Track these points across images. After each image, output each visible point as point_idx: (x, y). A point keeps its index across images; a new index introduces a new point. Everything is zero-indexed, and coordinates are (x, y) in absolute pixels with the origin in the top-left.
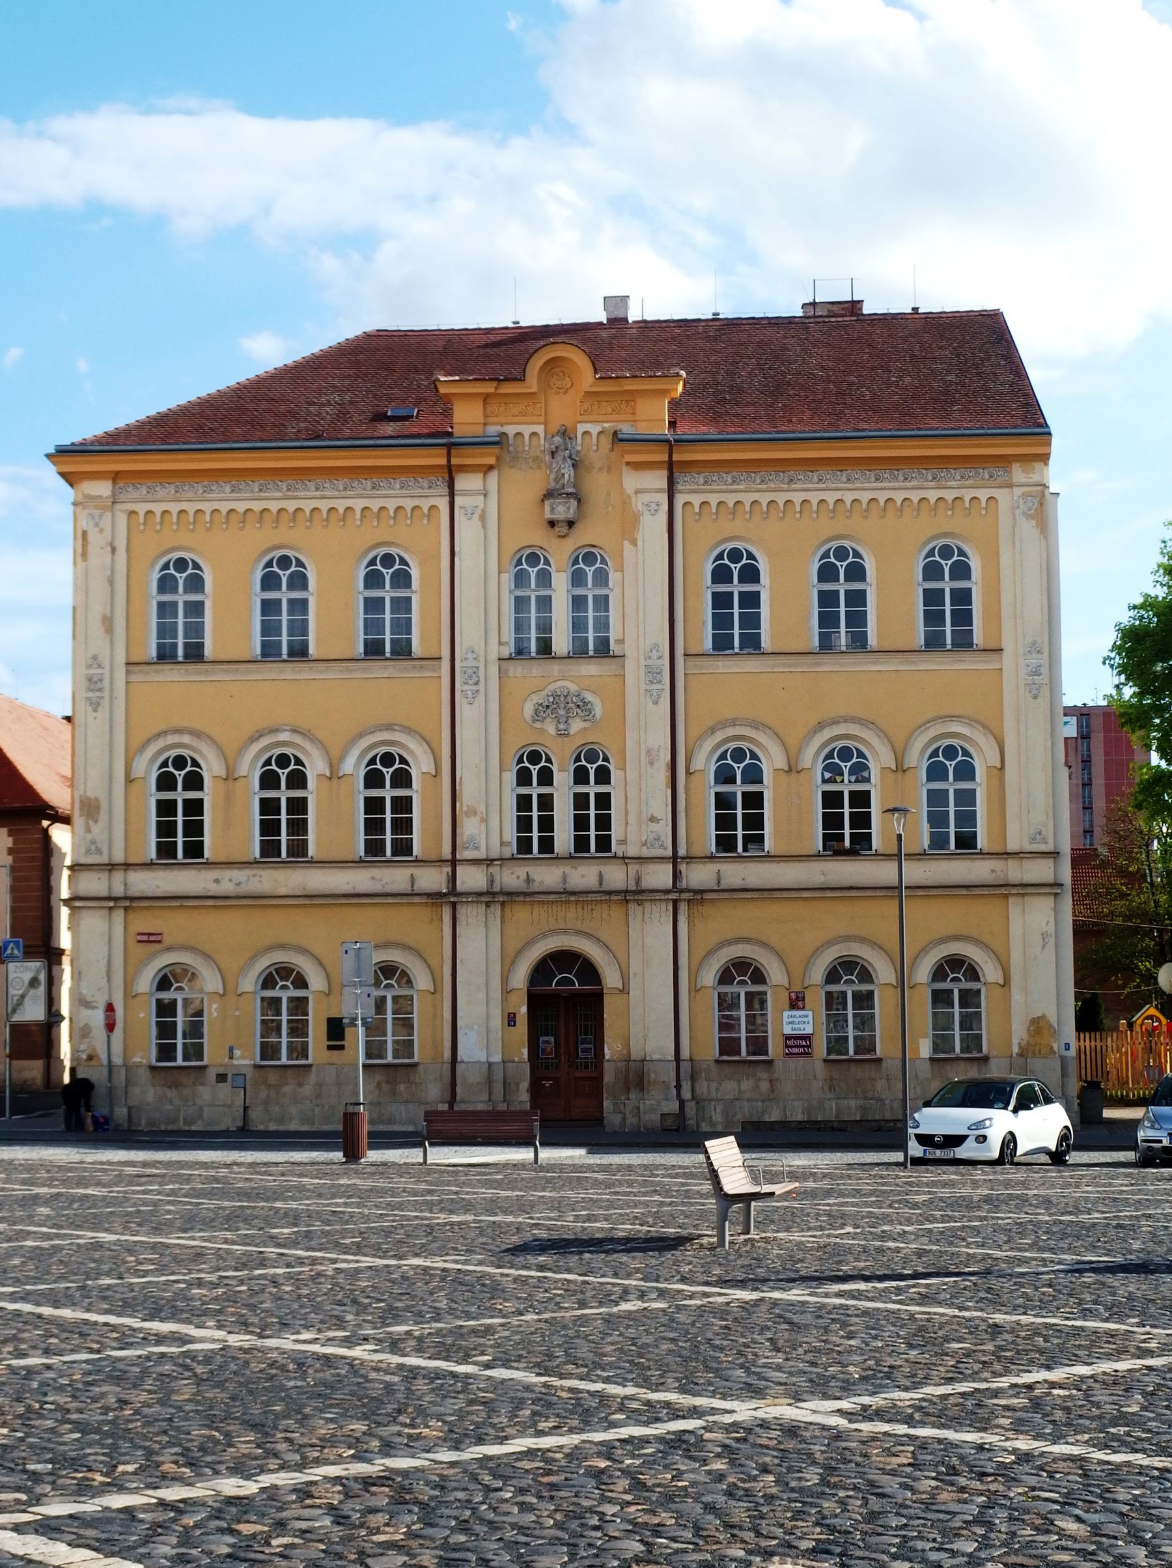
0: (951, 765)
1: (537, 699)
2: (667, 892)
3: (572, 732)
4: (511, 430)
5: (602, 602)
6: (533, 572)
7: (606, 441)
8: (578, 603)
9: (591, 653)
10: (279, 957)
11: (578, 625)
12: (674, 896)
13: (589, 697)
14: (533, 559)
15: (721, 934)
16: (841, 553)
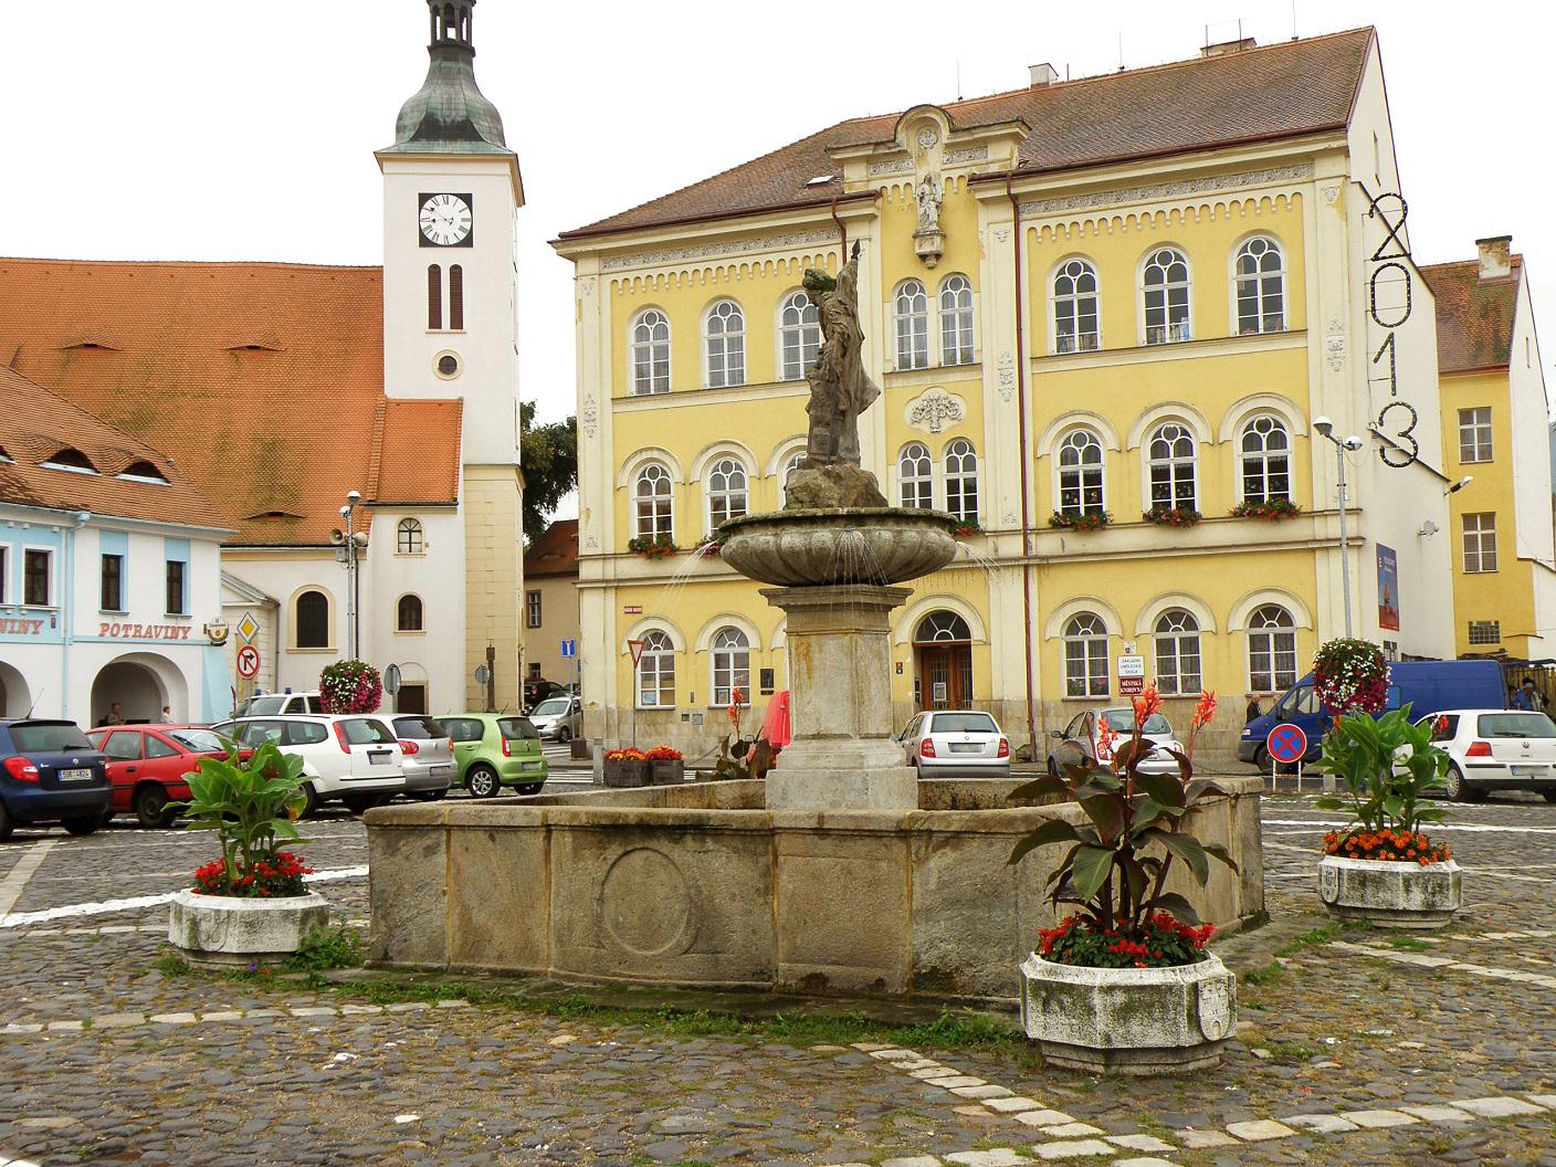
0: (1264, 436)
1: (917, 403)
2: (1019, 559)
3: (942, 429)
4: (889, 184)
5: (967, 320)
6: (911, 298)
7: (964, 183)
8: (948, 321)
9: (959, 363)
10: (727, 622)
11: (948, 339)
12: (1026, 562)
13: (955, 399)
14: (911, 289)
15: (1063, 593)
16: (1165, 258)
